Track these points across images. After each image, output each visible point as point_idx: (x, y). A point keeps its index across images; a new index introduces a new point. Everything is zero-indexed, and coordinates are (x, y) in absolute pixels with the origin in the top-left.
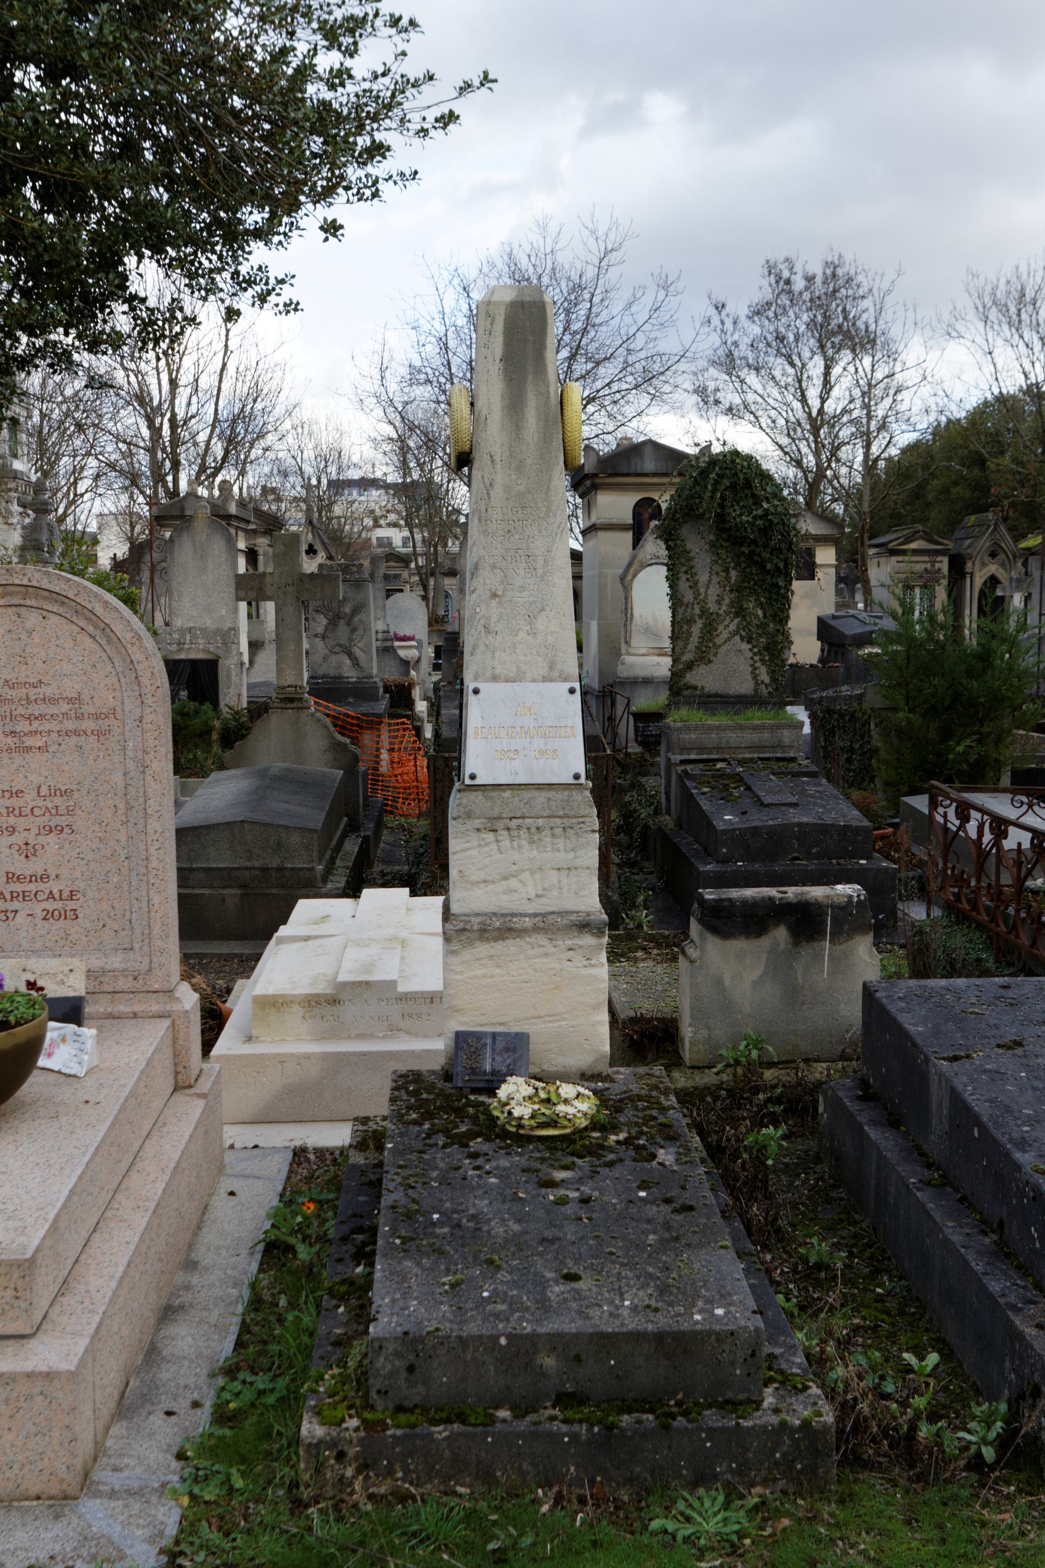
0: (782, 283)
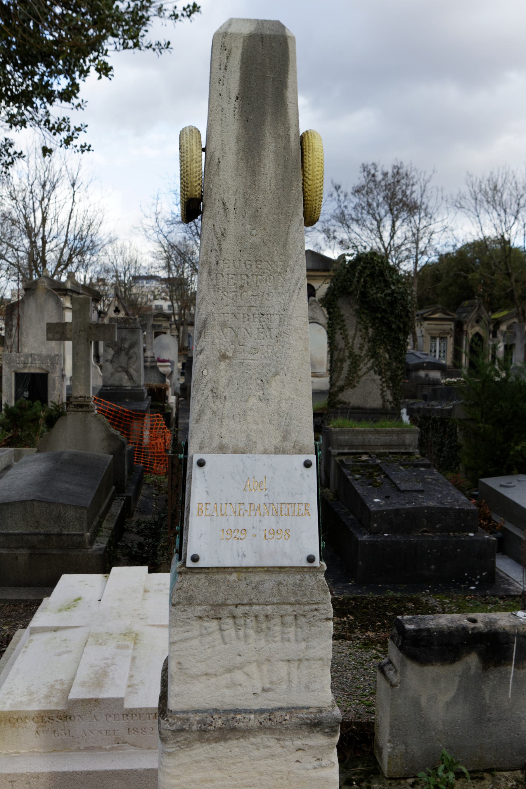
0: (370, 176)
